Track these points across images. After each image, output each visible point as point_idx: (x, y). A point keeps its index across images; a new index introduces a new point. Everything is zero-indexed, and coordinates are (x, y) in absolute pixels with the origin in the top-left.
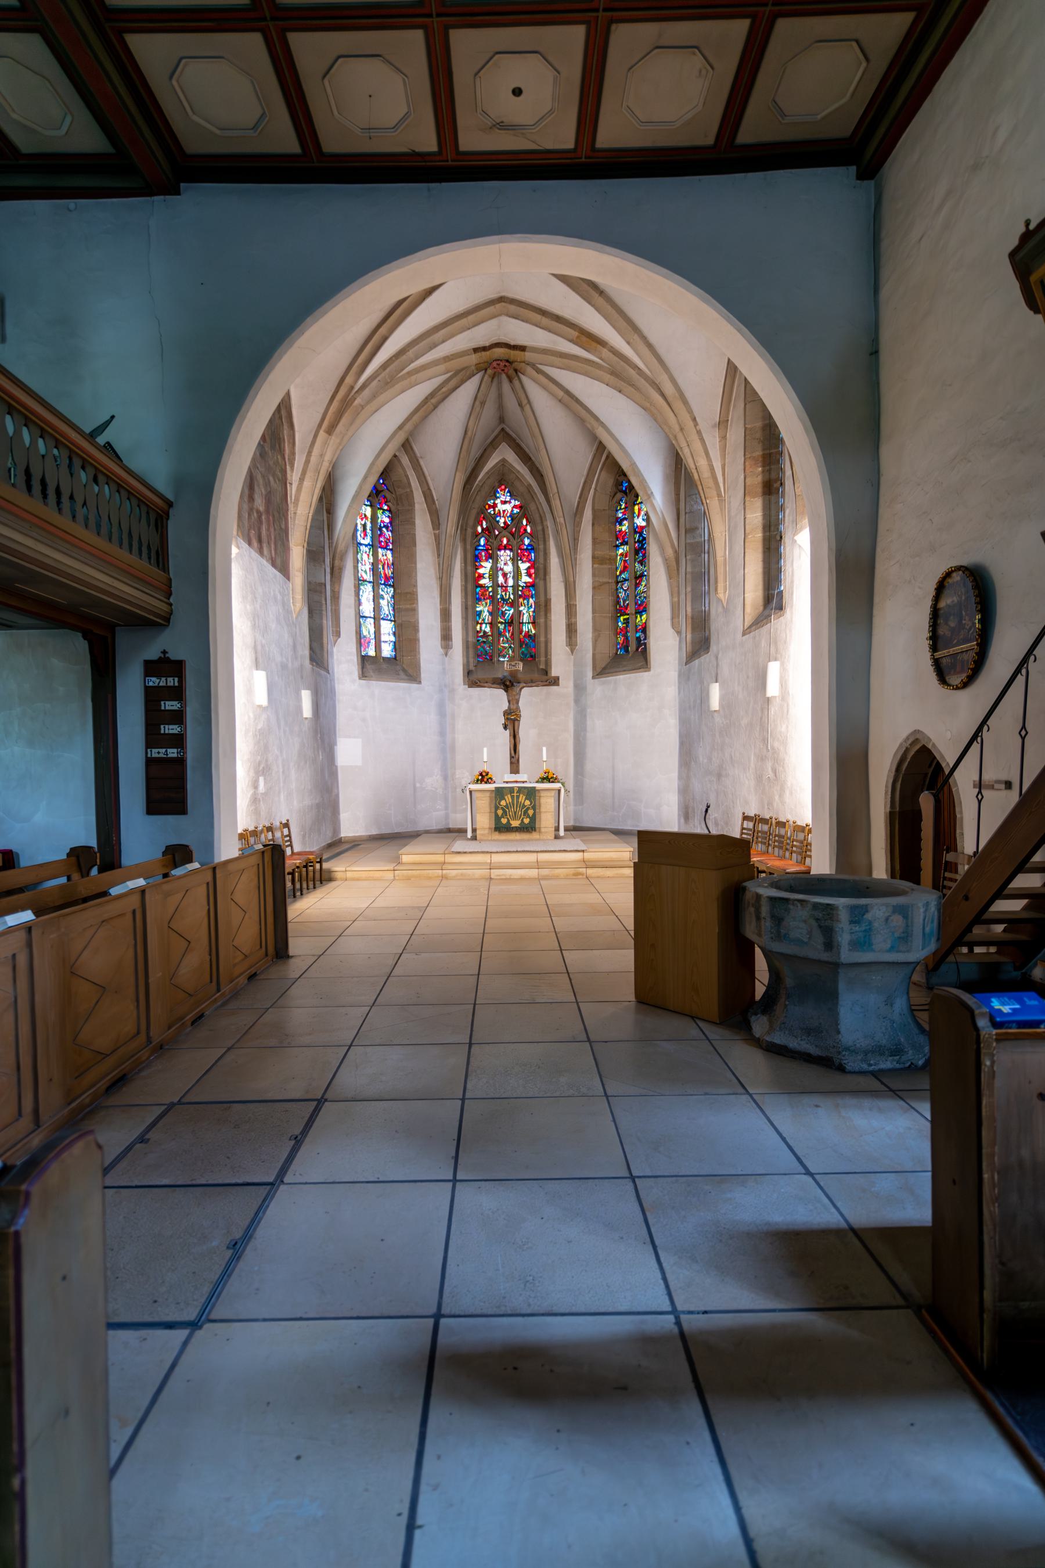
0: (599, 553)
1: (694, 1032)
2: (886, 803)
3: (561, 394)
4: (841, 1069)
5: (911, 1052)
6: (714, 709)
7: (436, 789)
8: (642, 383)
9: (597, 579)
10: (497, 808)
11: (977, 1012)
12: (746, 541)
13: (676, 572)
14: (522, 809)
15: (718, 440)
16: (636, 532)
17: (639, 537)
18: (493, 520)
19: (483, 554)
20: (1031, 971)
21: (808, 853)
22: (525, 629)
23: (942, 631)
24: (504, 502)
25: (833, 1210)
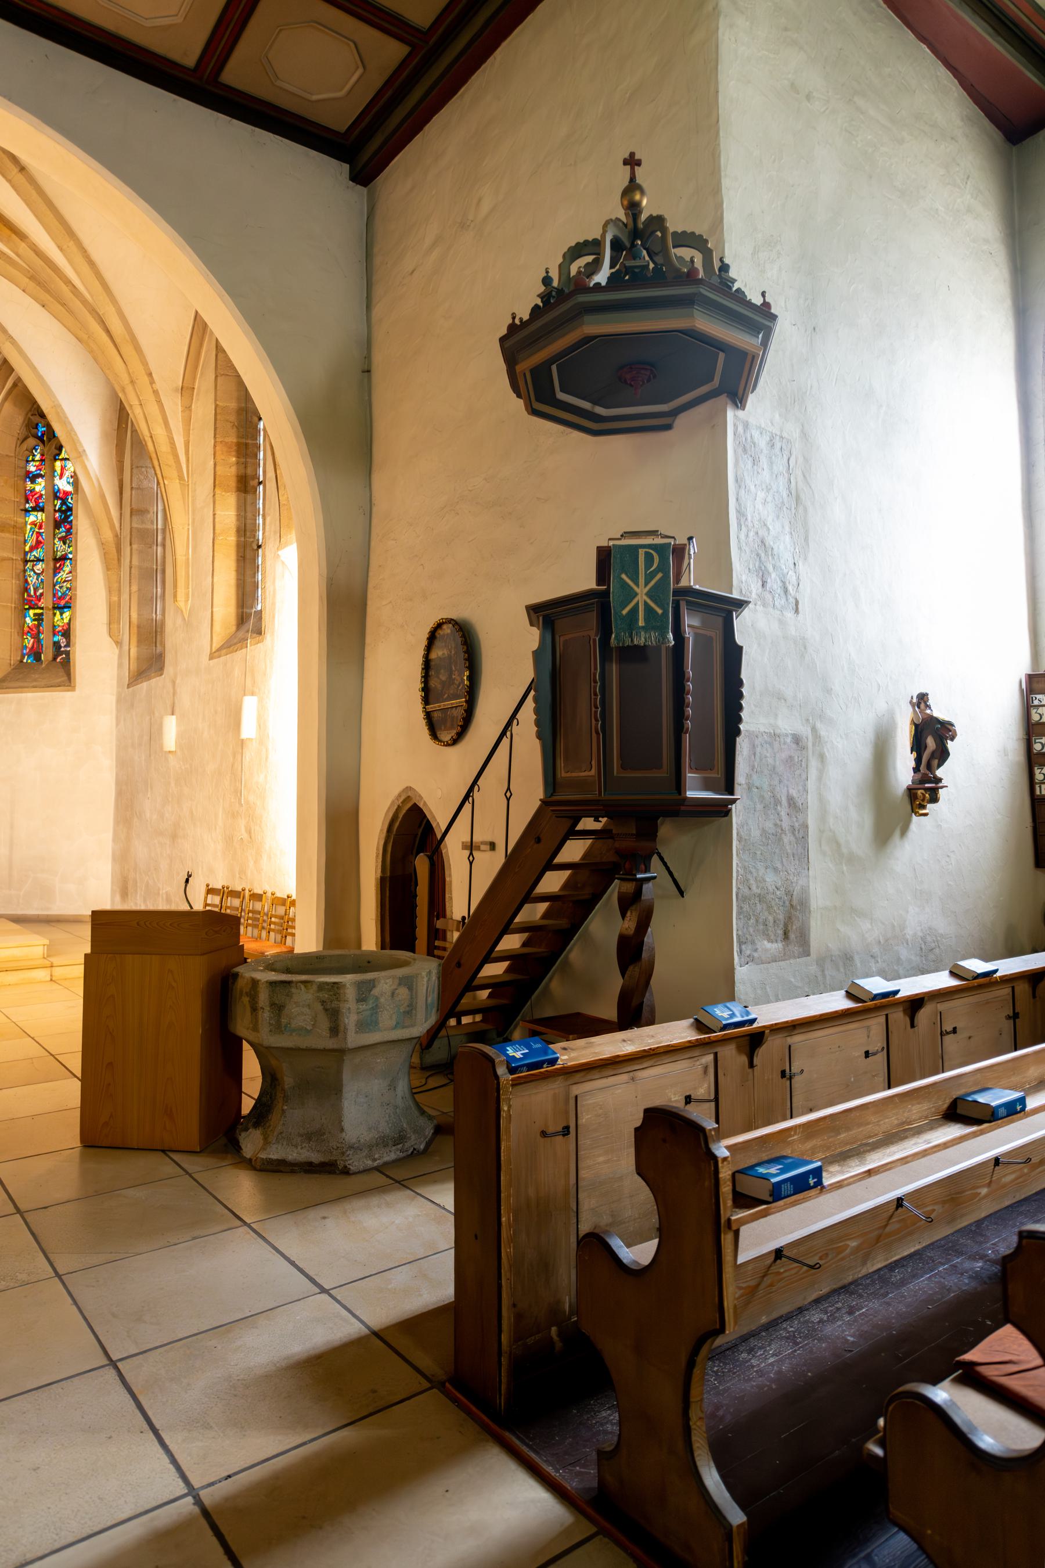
1: (169, 1168)
2: (377, 866)
4: (346, 1172)
5: (413, 1137)
6: (168, 750)
8: (76, 304)
11: (497, 1061)
12: (216, 542)
13: (116, 562)
15: (180, 409)
16: (56, 497)
17: (62, 504)
20: (511, 1036)
21: (290, 931)
23: (433, 683)
25: (354, 1320)
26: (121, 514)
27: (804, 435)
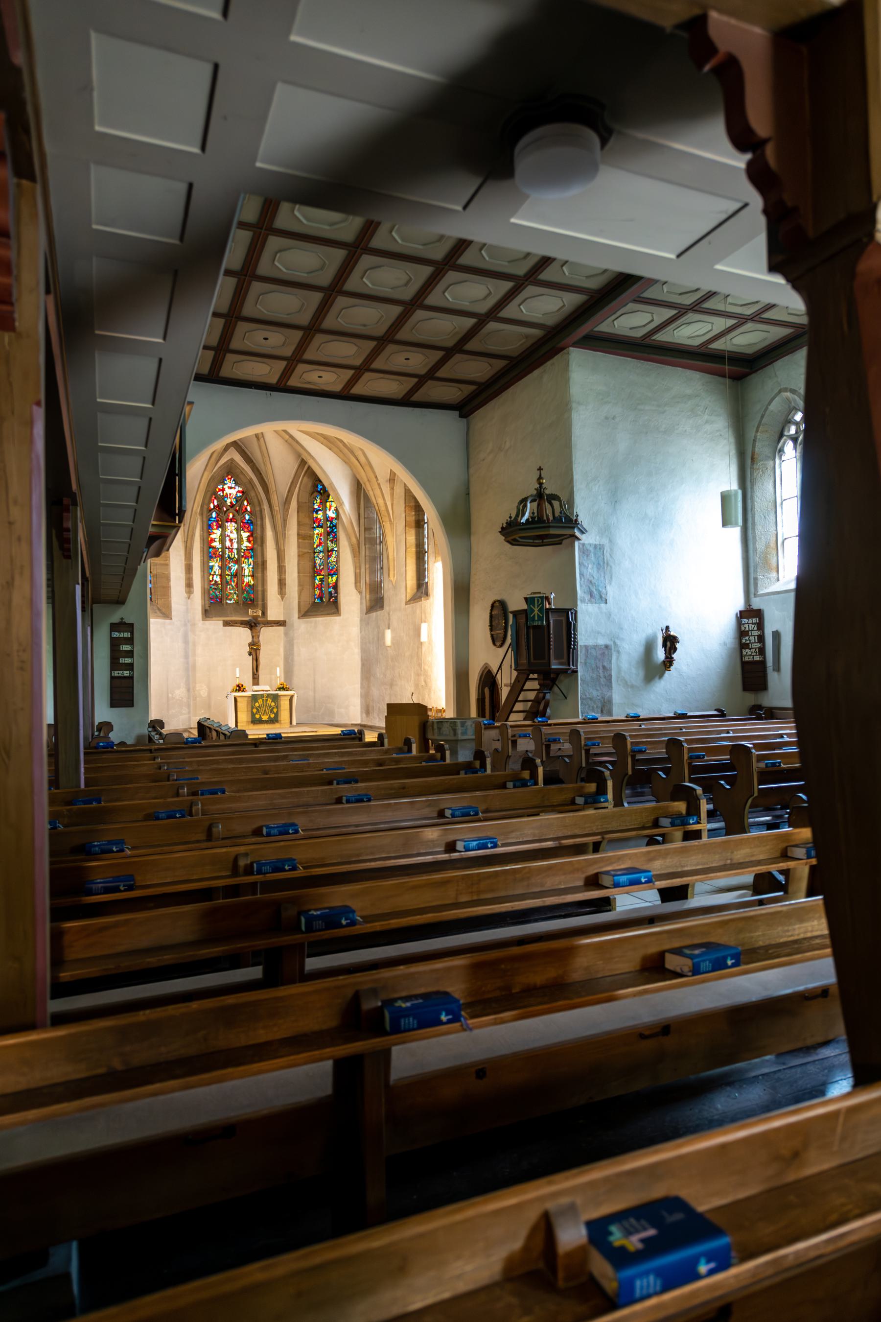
0: (303, 532)
3: (287, 437)
7: (182, 698)
9: (301, 550)
10: (253, 708)
13: (358, 553)
14: (270, 708)
17: (330, 524)
18: (222, 500)
19: (215, 524)
22: (246, 580)
23: (494, 623)
24: (230, 488)
26: (360, 529)
27: (610, 541)
